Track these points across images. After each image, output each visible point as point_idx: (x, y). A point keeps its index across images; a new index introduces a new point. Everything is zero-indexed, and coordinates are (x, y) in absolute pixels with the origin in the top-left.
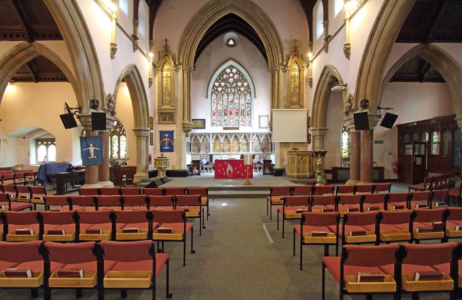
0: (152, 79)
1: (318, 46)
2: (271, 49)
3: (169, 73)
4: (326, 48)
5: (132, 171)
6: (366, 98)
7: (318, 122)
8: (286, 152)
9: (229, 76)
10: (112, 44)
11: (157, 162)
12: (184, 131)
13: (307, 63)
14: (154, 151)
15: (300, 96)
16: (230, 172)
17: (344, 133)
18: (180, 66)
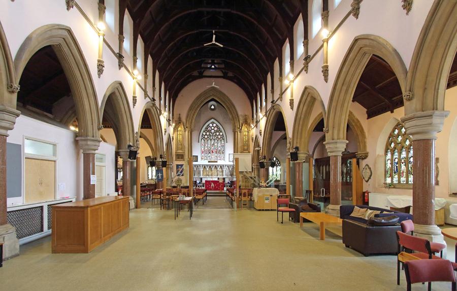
4: (306, 68)
15: (248, 146)
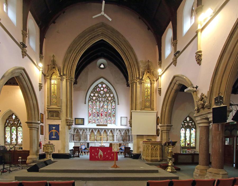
0: (42, 84)
1: (165, 64)
2: (131, 67)
3: (56, 81)
4: (175, 62)
5: (26, 154)
6: (220, 95)
7: (166, 120)
8: (141, 142)
9: (100, 89)
10: (39, 84)
11: (45, 147)
12: (67, 125)
13: (156, 78)
14: (43, 139)
15: (151, 102)
16: (101, 155)
17: (182, 129)
18: (64, 77)
